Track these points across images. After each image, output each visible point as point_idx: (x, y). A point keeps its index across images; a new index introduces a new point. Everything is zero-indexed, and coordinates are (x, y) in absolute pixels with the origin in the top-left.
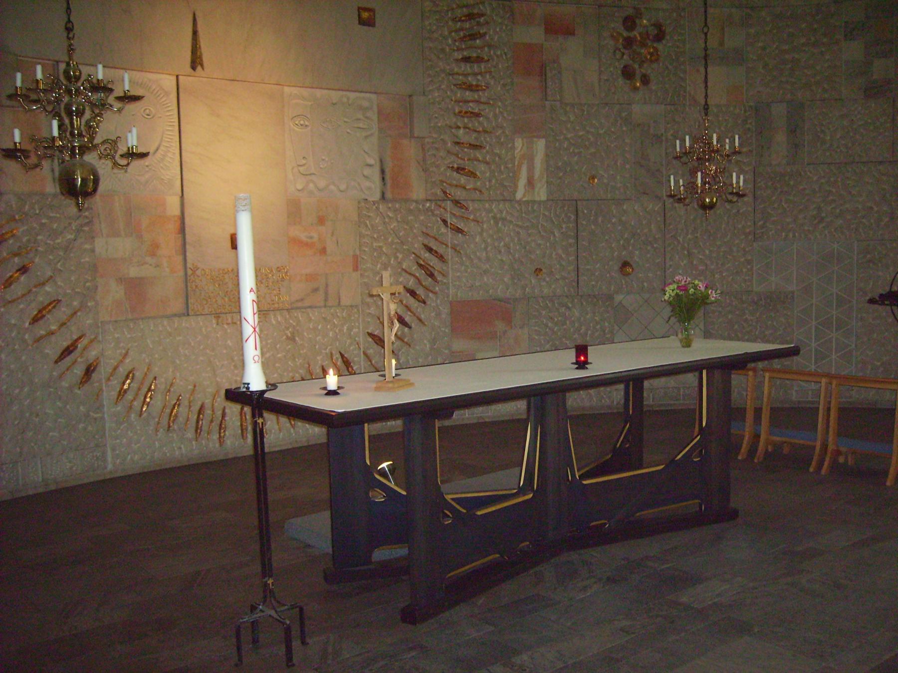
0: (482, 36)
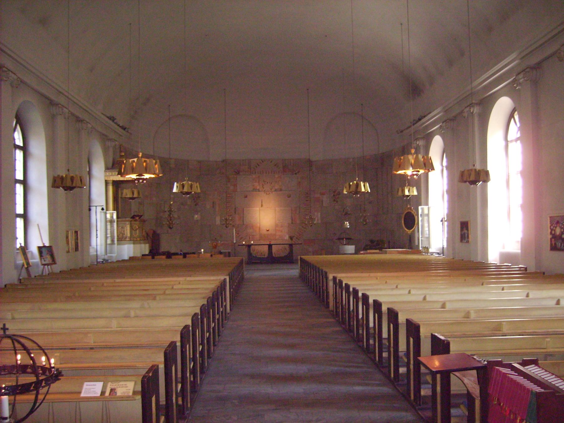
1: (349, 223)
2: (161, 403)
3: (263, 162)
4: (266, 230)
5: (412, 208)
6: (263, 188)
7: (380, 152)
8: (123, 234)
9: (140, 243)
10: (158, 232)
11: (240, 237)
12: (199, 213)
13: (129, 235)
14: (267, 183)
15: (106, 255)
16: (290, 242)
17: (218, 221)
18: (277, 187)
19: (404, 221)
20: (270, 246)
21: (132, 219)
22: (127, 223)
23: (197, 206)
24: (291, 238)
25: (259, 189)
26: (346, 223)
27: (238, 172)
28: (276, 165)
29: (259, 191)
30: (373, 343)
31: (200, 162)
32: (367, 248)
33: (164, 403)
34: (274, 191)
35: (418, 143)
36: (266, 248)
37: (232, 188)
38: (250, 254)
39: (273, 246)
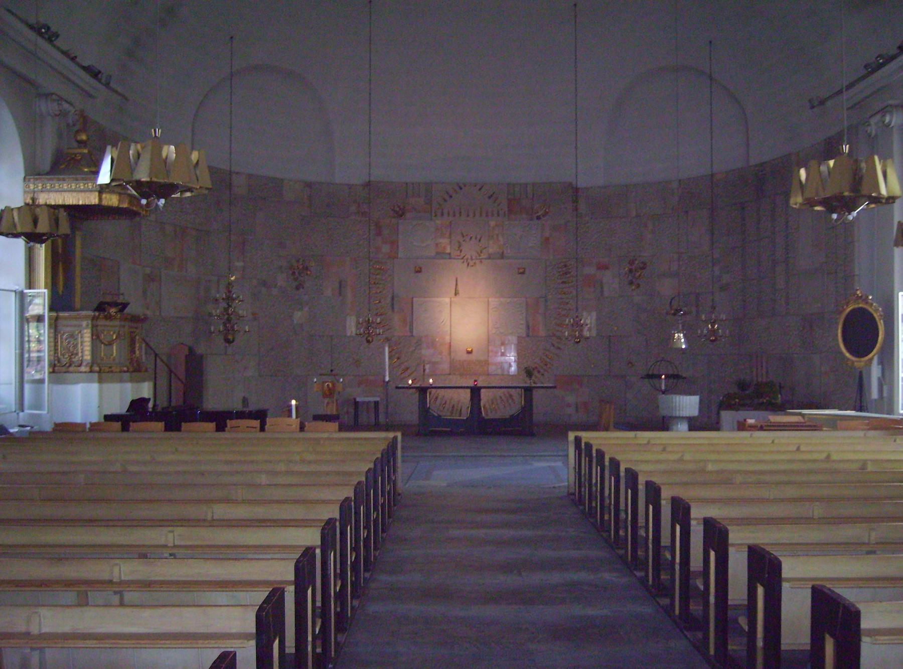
0: (570, 273)
1: (685, 336)
2: (287, 651)
3: (461, 188)
4: (465, 352)
5: (870, 297)
6: (461, 251)
7: (753, 162)
8: (73, 354)
9: (121, 381)
10: (201, 350)
11: (403, 367)
12: (306, 309)
13: (88, 357)
14: (471, 238)
15: (23, 411)
16: (528, 383)
17: (351, 327)
18: (493, 249)
19: (844, 332)
20: (475, 391)
21: (97, 314)
22: (84, 323)
23: (301, 290)
24: (529, 373)
25: (450, 254)
26: (676, 335)
27: (400, 213)
28: (491, 196)
29: (450, 258)
30: (624, 534)
31: (309, 185)
32: (733, 403)
33: (293, 651)
34: (486, 259)
35: (887, 119)
36: (466, 395)
37: (386, 249)
38: (424, 409)
39: (483, 391)
